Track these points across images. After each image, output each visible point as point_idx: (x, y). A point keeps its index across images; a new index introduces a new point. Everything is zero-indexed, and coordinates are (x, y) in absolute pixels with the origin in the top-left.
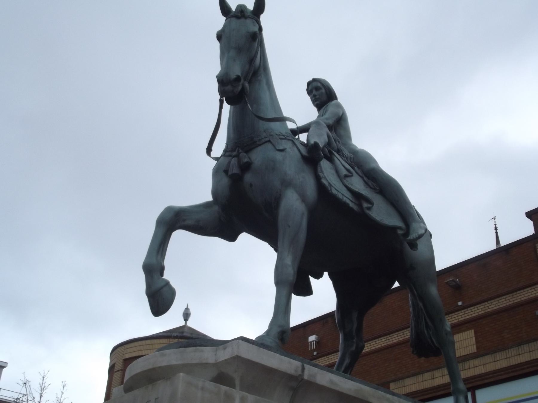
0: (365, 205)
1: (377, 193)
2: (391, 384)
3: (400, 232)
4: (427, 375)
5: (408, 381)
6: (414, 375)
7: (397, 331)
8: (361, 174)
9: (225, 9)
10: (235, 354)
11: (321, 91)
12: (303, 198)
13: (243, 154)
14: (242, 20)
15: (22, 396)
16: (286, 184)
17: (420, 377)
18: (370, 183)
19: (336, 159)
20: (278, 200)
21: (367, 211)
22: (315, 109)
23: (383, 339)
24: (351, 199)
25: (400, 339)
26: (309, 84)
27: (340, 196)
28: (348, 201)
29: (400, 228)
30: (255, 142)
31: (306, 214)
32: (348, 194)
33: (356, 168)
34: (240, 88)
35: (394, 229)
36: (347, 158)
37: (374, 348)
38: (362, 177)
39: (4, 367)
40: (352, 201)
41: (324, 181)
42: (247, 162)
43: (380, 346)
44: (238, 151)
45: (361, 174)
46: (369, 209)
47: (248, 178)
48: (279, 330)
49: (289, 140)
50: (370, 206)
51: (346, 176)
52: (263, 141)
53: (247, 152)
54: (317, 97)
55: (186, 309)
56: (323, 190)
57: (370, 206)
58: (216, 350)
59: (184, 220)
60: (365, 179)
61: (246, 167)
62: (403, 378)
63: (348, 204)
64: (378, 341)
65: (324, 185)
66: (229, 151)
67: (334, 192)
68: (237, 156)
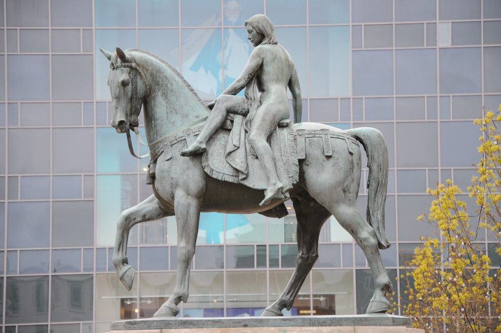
16: (175, 186)
21: (242, 182)
59: (135, 219)
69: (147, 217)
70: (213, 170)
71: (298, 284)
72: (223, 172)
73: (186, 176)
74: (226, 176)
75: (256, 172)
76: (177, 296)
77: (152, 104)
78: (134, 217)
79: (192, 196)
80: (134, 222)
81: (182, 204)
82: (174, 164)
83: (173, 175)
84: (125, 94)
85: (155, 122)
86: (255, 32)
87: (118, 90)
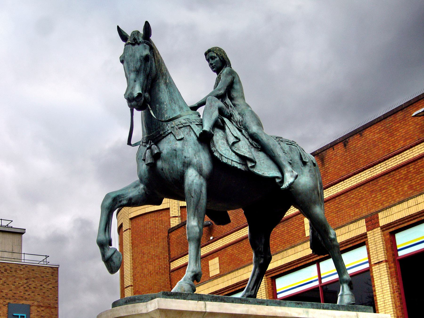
0: (250, 165)
1: (260, 151)
2: (379, 214)
3: (278, 181)
4: (411, 202)
5: (395, 209)
6: (400, 203)
7: (380, 162)
8: (247, 137)
9: (123, 36)
10: (157, 308)
11: (216, 59)
12: (200, 172)
13: (154, 147)
14: (136, 46)
15: (45, 257)
16: (187, 165)
17: (405, 205)
18: (254, 143)
19: (226, 127)
20: (182, 177)
21: (252, 169)
22: (215, 74)
23: (367, 171)
24: (239, 162)
25: (383, 170)
26: (206, 54)
27: (229, 163)
28: (236, 165)
29: (278, 177)
30: (162, 135)
31: (204, 184)
32: (236, 158)
33: (243, 131)
34: (143, 99)
35: (274, 178)
36: (236, 122)
37: (360, 181)
38: (248, 139)
39: (23, 233)
40: (239, 163)
41: (216, 154)
42: (157, 153)
43: (365, 179)
44: (150, 143)
45: (247, 137)
46: (253, 167)
47: (159, 164)
48: (192, 274)
49: (186, 126)
50: (253, 164)
51: (234, 143)
52: (167, 133)
53: (156, 143)
54: (213, 65)
55: (231, 65)
56: (215, 161)
57: (253, 164)
58: (146, 305)
59: (120, 202)
60: (250, 140)
61: (157, 156)
62: (390, 207)
63: (236, 167)
64: (362, 174)
65: (217, 157)
66: (145, 143)
67: (225, 160)
68: (150, 148)
69: (133, 201)
70: (222, 155)
71: (317, 257)
72: (231, 159)
73: (198, 157)
74: (235, 163)
75: (262, 161)
76: (194, 274)
77: (157, 89)
78: (120, 199)
79: (204, 177)
80: (119, 204)
81: (196, 183)
82: (186, 144)
83: (186, 154)
84: (145, 70)
85: (160, 105)
86: (218, 59)
87: (139, 64)
